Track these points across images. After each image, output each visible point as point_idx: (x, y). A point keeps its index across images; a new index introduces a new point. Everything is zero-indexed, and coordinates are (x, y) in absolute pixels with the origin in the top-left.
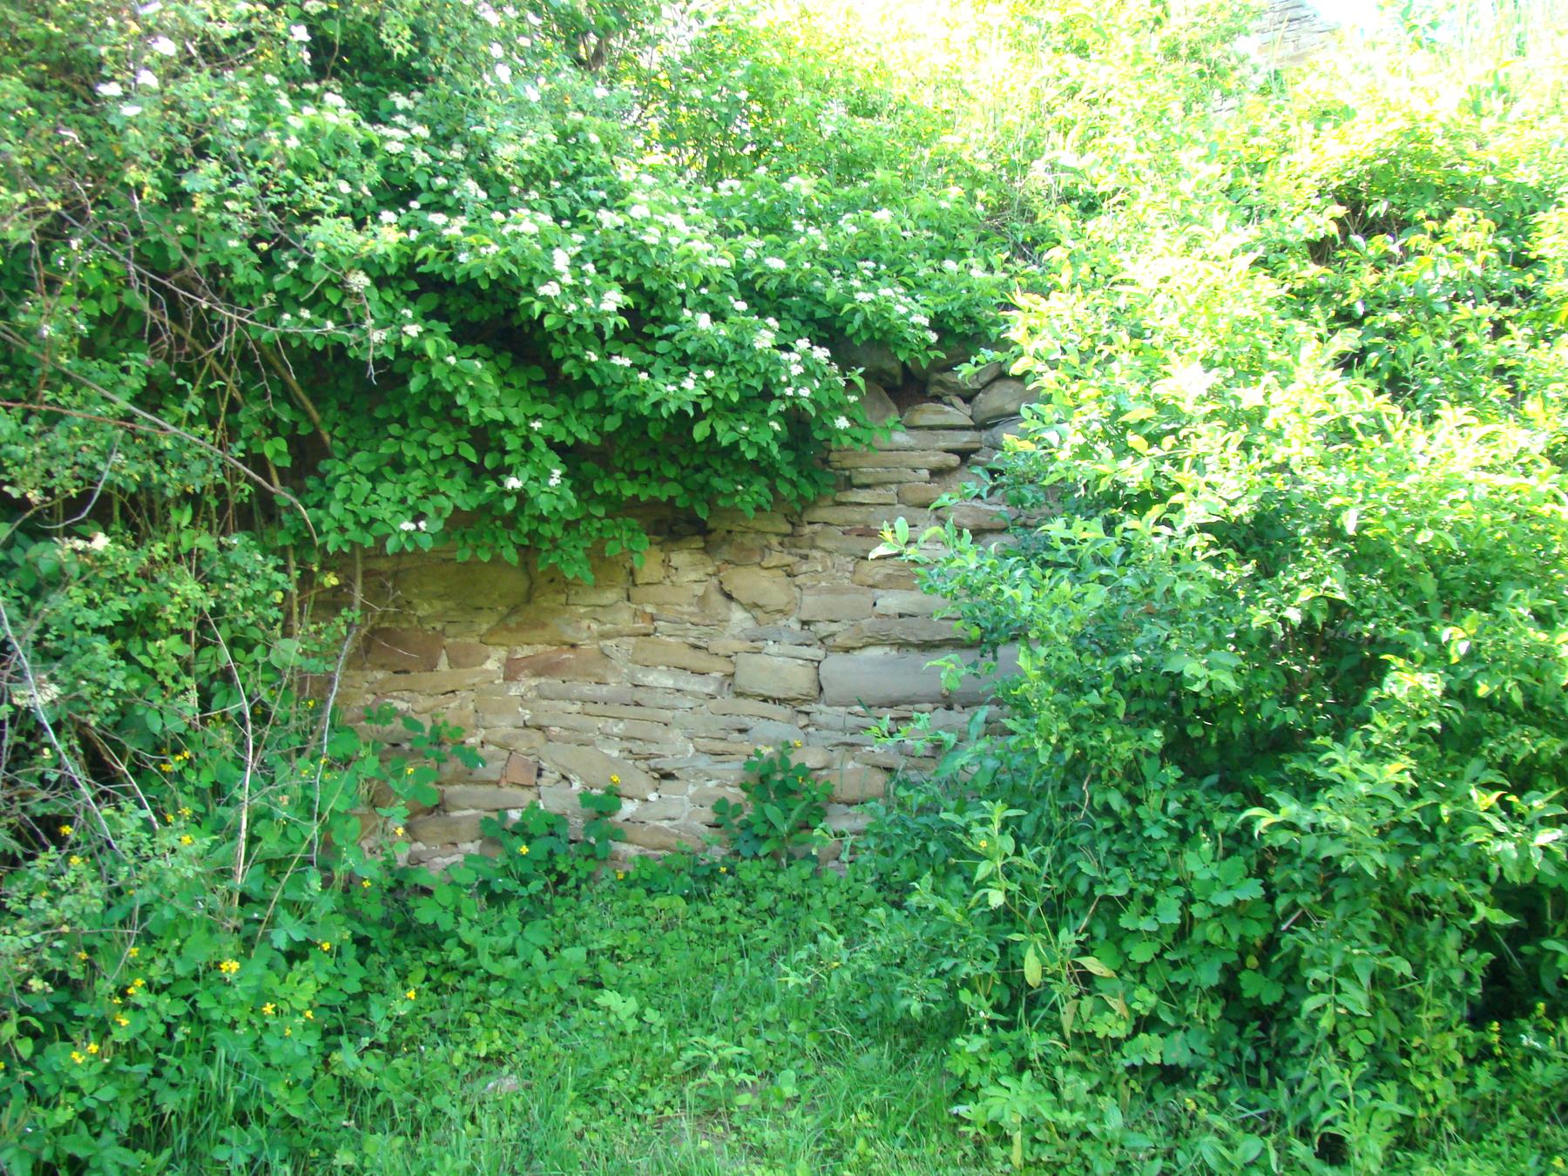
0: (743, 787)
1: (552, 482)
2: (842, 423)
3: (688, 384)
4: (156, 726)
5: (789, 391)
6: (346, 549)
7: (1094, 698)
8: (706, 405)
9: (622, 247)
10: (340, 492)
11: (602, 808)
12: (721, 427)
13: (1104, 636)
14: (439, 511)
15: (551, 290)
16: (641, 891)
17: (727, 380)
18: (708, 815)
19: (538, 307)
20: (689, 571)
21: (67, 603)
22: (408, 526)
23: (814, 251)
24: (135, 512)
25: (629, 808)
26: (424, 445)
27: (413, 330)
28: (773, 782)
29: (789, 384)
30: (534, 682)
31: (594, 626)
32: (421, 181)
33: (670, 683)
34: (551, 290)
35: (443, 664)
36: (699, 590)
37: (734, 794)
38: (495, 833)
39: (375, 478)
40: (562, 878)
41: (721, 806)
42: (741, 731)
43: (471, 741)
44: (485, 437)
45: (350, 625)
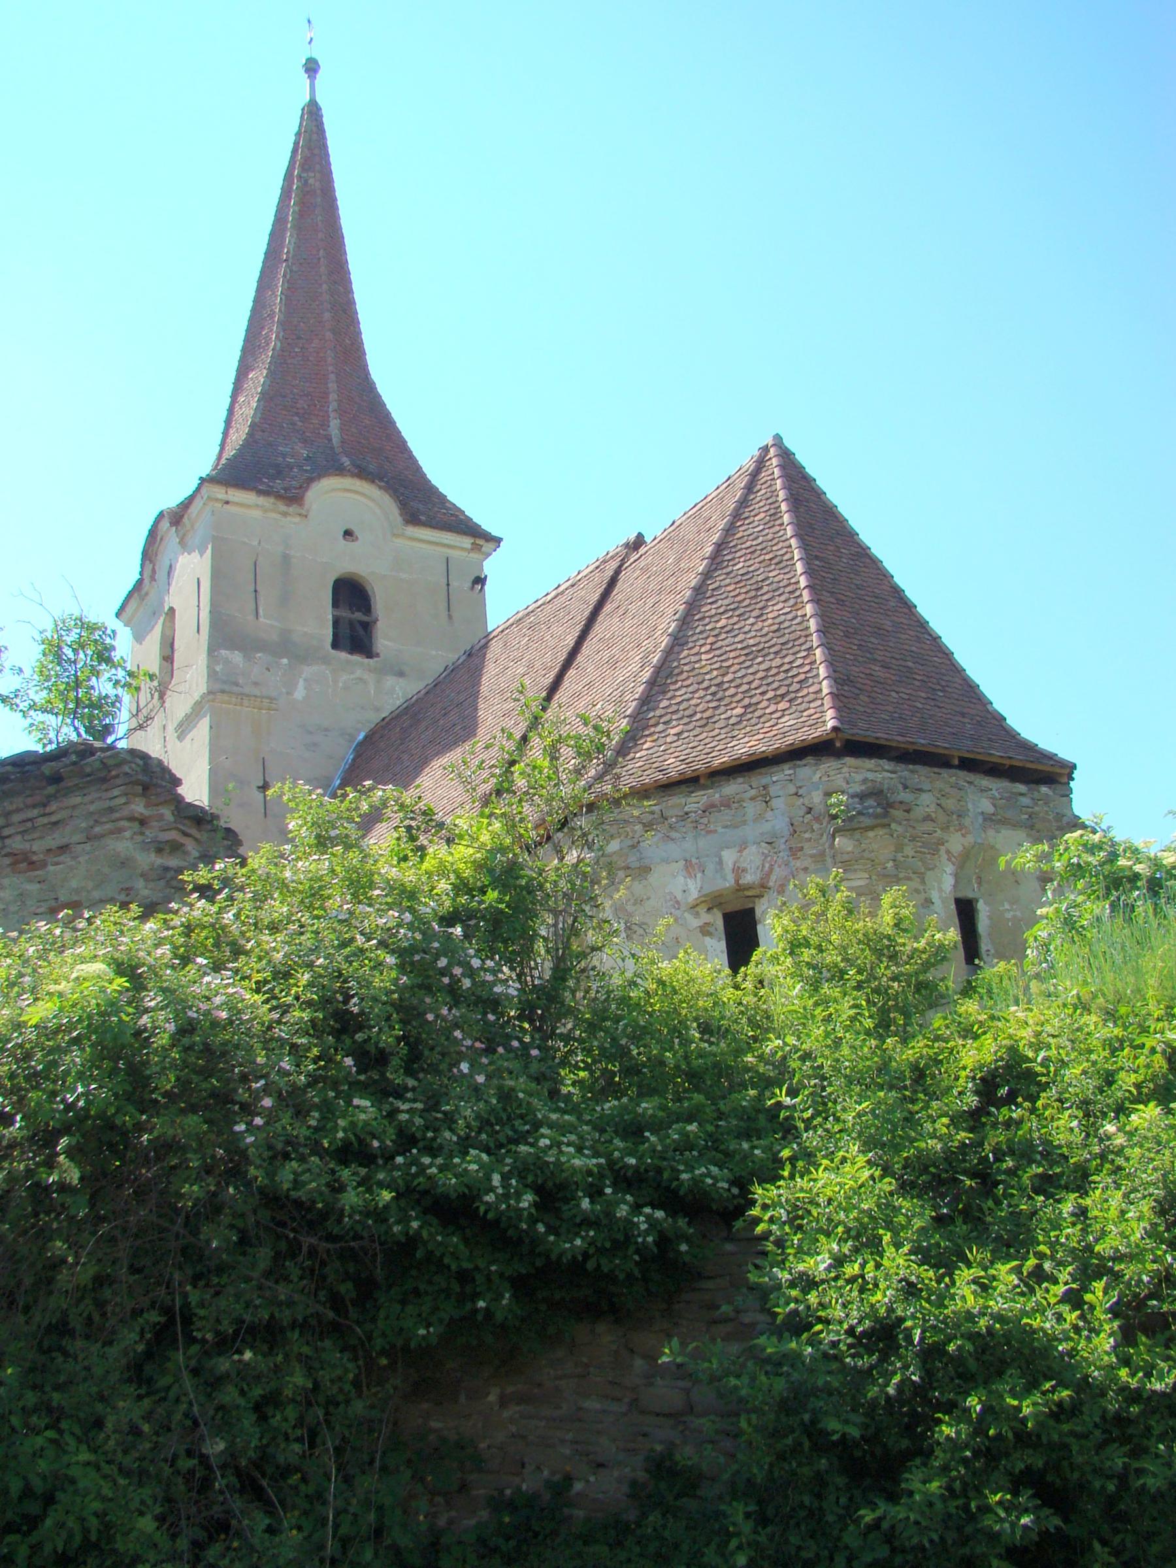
0: (646, 1470)
1: (504, 1302)
2: (684, 1247)
3: (578, 1242)
4: (281, 1459)
5: (640, 1240)
6: (387, 1347)
7: (789, 1441)
8: (591, 1251)
9: (534, 1164)
10: (382, 1314)
11: (561, 1488)
12: (604, 1261)
13: (786, 1407)
14: (441, 1321)
15: (490, 1198)
16: (580, 1542)
17: (602, 1235)
18: (625, 1489)
19: (482, 1209)
20: (606, 1336)
21: (229, 1395)
22: (422, 1332)
23: (654, 1151)
24: (268, 1335)
25: (578, 1486)
26: (430, 1282)
27: (415, 1224)
28: (662, 1467)
29: (639, 1235)
30: (517, 1408)
31: (552, 1372)
32: (419, 1135)
33: (598, 1406)
34: (490, 1198)
35: (462, 1399)
36: (614, 1347)
37: (641, 1476)
38: (498, 1504)
39: (404, 1302)
40: (536, 1534)
41: (634, 1483)
42: (645, 1435)
43: (482, 1445)
44: (464, 1277)
45: (395, 1388)
